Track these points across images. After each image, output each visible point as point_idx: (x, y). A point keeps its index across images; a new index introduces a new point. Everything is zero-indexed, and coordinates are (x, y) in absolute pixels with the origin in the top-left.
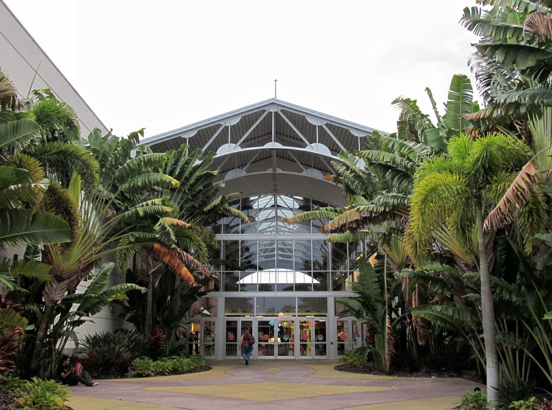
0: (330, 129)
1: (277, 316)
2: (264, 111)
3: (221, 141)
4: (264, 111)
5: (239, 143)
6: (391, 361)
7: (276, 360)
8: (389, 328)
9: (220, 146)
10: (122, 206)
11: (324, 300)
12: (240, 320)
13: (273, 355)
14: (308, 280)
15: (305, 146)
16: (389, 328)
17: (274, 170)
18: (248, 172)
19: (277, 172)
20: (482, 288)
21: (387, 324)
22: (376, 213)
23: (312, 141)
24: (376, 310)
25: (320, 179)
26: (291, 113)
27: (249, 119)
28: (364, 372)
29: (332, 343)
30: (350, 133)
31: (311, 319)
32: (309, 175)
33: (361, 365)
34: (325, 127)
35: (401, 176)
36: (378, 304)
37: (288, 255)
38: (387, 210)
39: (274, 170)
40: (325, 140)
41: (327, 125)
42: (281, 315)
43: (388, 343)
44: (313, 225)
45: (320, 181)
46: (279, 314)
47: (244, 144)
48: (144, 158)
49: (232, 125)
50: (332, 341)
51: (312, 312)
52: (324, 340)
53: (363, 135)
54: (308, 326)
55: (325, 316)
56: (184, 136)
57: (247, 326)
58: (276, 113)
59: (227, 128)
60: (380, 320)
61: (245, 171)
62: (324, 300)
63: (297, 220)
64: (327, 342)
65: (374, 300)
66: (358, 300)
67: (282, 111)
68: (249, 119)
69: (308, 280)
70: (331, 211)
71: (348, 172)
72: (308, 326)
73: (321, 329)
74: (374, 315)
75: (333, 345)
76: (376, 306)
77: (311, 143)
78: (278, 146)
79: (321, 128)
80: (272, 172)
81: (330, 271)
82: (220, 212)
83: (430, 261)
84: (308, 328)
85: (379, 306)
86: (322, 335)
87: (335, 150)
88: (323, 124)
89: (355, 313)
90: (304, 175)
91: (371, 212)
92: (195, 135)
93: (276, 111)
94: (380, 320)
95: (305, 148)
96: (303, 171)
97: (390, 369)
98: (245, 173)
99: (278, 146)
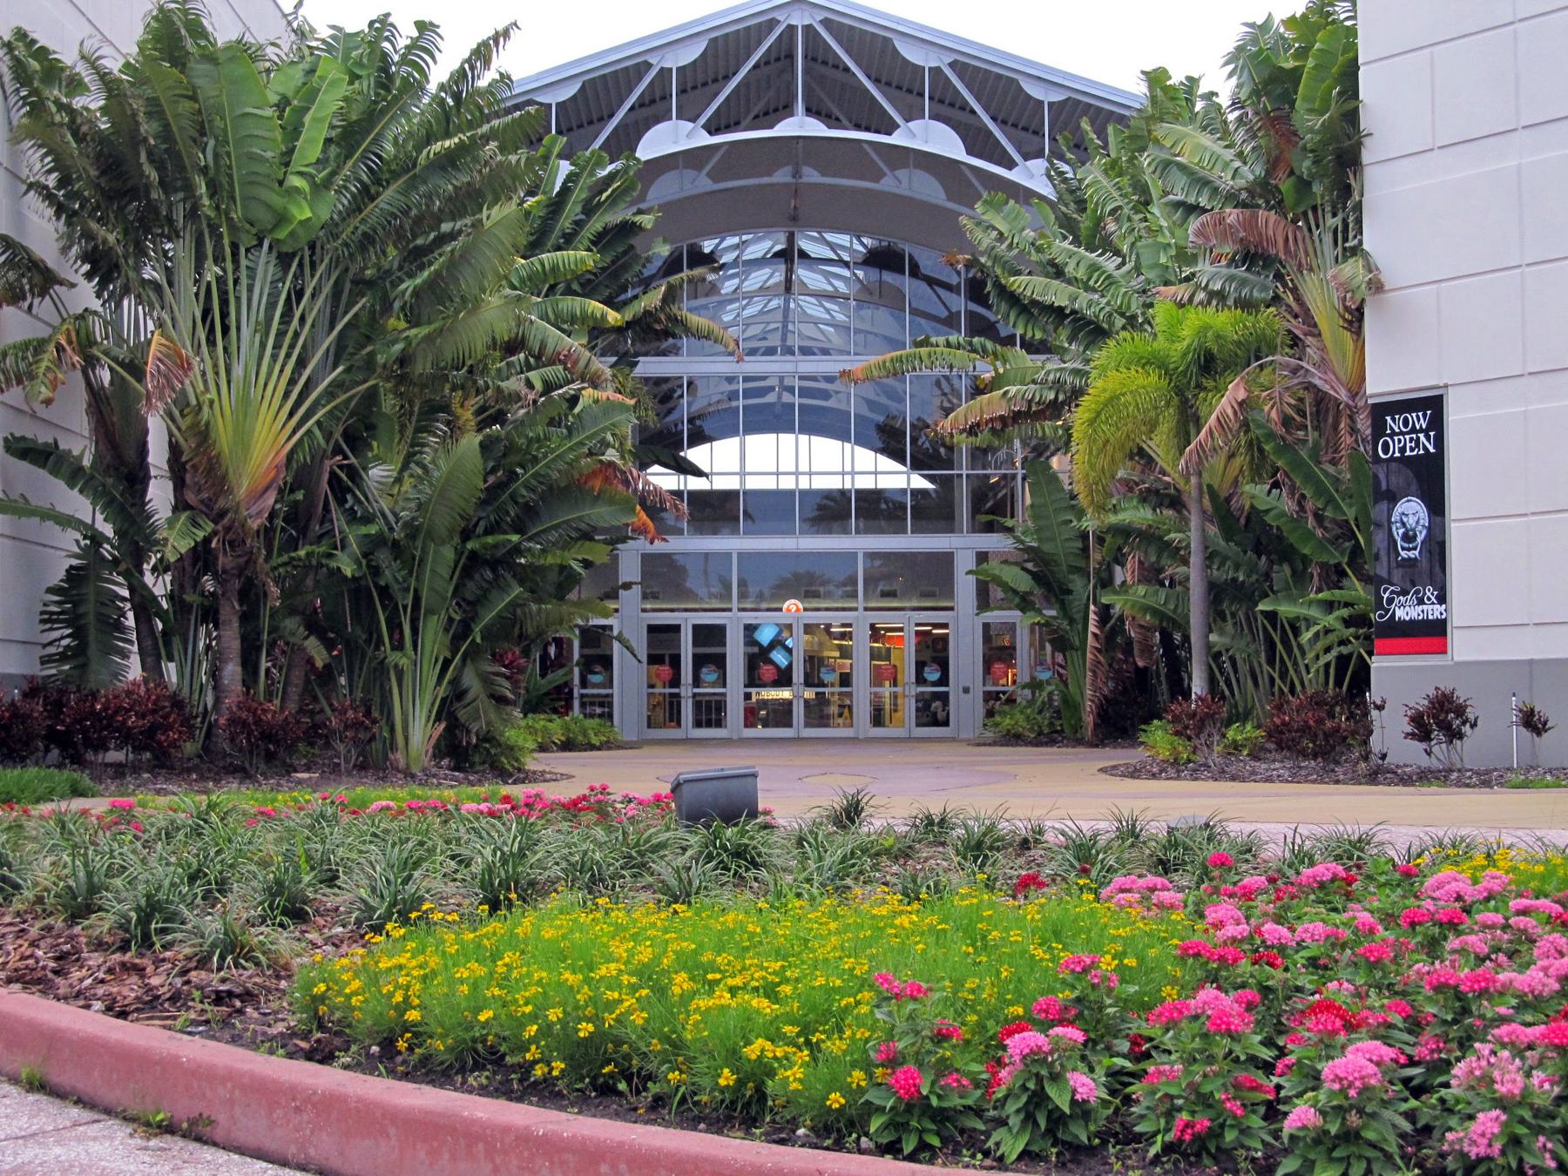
0: (961, 78)
1: (780, 610)
2: (773, 23)
3: (652, 110)
4: (773, 23)
5: (703, 120)
6: (1099, 715)
7: (798, 740)
8: (1095, 635)
9: (648, 128)
10: (232, 227)
11: (944, 562)
12: (688, 621)
13: (790, 725)
14: (894, 477)
15: (889, 127)
16: (1095, 635)
17: (796, 174)
18: (715, 179)
19: (805, 180)
20: (1192, 560)
21: (1092, 628)
22: (1038, 403)
23: (911, 114)
24: (1070, 592)
25: (934, 201)
26: (851, 28)
27: (727, 52)
28: (1037, 745)
29: (966, 690)
30: (1021, 89)
31: (906, 621)
32: (903, 190)
33: (1031, 730)
34: (948, 72)
35: (1091, 332)
36: (1075, 577)
37: (819, 390)
38: (1061, 397)
39: (796, 174)
40: (949, 109)
41: (952, 65)
42: (794, 608)
43: (1094, 672)
44: (914, 312)
45: (936, 207)
46: (785, 606)
47: (712, 129)
48: (543, 265)
49: (681, 64)
50: (968, 684)
51: (906, 594)
52: (944, 681)
53: (1057, 97)
54: (889, 650)
55: (951, 609)
56: (543, 98)
57: (710, 636)
58: (808, 29)
59: (664, 73)
60: (1078, 616)
61: (708, 175)
62: (944, 562)
63: (875, 373)
64: (953, 689)
65: (1064, 568)
66: (1024, 569)
67: (826, 23)
68: (727, 52)
69: (894, 477)
70: (959, 347)
71: (1004, 246)
72: (889, 650)
73: (934, 650)
74: (1063, 607)
75: (970, 696)
76: (1072, 581)
77: (908, 121)
78: (816, 128)
79: (936, 72)
80: (789, 179)
81: (964, 472)
82: (657, 327)
83: (1135, 502)
84: (888, 658)
85: (1077, 583)
86: (935, 666)
87: (978, 141)
88: (941, 61)
89: (1017, 600)
90: (887, 189)
91: (1030, 402)
92: (574, 97)
93: (807, 22)
94: (1078, 616)
95: (889, 134)
96: (884, 175)
97: (1094, 733)
98: (709, 182)
99: (816, 128)
